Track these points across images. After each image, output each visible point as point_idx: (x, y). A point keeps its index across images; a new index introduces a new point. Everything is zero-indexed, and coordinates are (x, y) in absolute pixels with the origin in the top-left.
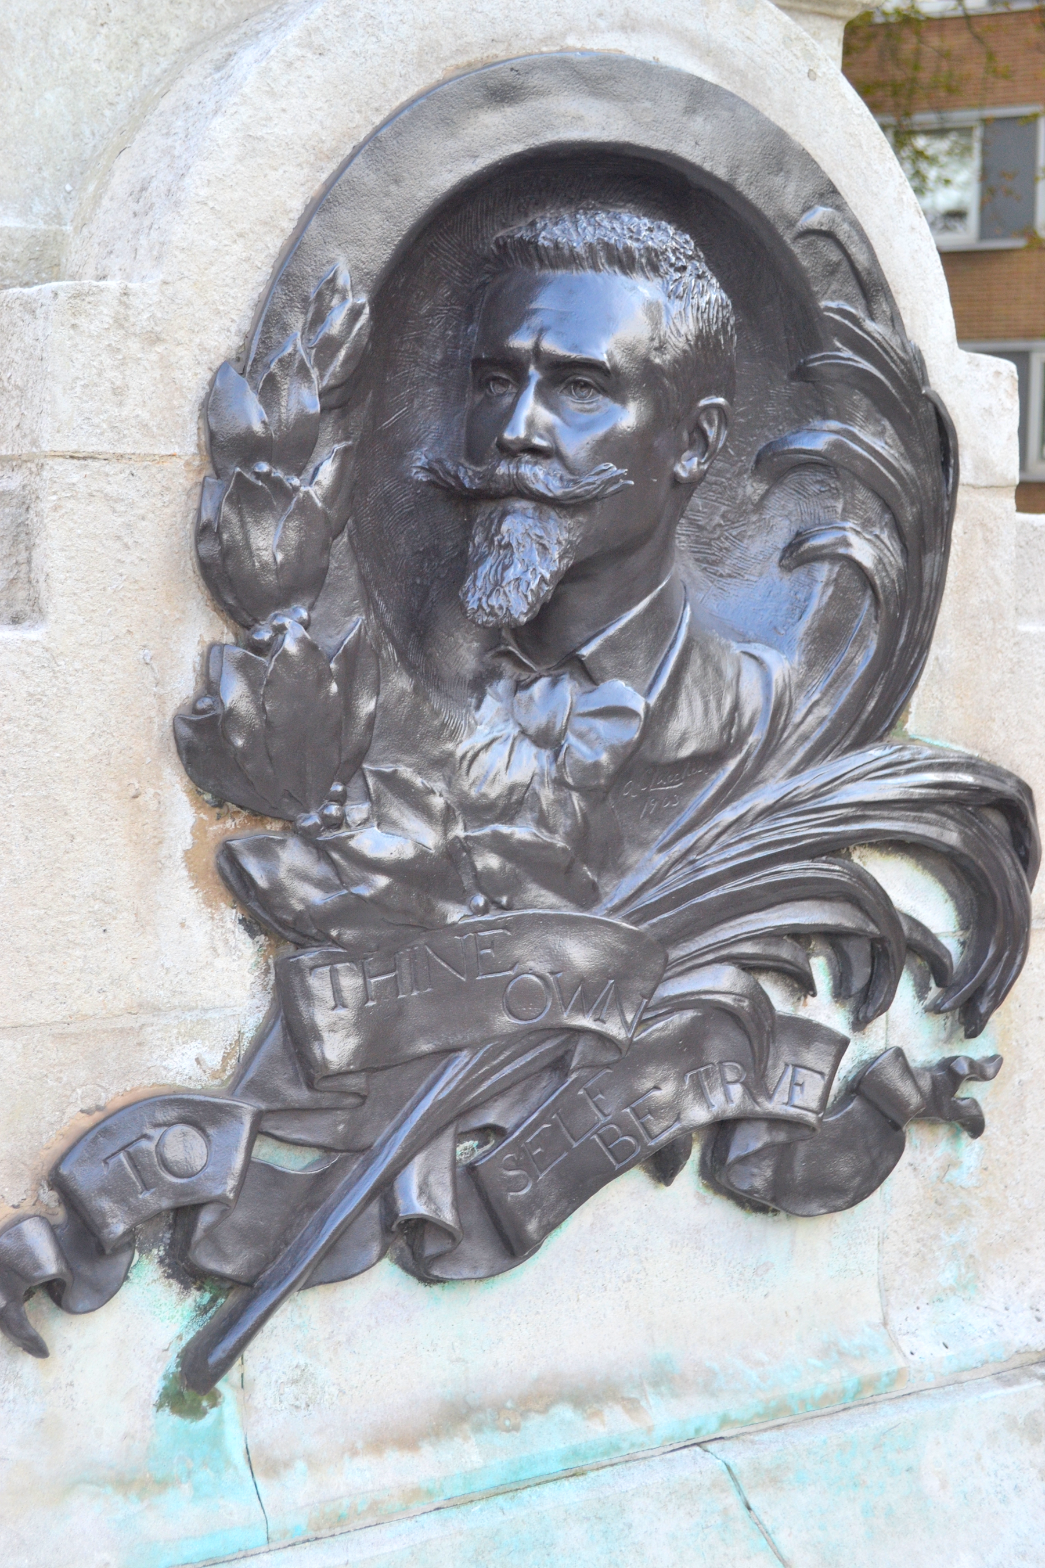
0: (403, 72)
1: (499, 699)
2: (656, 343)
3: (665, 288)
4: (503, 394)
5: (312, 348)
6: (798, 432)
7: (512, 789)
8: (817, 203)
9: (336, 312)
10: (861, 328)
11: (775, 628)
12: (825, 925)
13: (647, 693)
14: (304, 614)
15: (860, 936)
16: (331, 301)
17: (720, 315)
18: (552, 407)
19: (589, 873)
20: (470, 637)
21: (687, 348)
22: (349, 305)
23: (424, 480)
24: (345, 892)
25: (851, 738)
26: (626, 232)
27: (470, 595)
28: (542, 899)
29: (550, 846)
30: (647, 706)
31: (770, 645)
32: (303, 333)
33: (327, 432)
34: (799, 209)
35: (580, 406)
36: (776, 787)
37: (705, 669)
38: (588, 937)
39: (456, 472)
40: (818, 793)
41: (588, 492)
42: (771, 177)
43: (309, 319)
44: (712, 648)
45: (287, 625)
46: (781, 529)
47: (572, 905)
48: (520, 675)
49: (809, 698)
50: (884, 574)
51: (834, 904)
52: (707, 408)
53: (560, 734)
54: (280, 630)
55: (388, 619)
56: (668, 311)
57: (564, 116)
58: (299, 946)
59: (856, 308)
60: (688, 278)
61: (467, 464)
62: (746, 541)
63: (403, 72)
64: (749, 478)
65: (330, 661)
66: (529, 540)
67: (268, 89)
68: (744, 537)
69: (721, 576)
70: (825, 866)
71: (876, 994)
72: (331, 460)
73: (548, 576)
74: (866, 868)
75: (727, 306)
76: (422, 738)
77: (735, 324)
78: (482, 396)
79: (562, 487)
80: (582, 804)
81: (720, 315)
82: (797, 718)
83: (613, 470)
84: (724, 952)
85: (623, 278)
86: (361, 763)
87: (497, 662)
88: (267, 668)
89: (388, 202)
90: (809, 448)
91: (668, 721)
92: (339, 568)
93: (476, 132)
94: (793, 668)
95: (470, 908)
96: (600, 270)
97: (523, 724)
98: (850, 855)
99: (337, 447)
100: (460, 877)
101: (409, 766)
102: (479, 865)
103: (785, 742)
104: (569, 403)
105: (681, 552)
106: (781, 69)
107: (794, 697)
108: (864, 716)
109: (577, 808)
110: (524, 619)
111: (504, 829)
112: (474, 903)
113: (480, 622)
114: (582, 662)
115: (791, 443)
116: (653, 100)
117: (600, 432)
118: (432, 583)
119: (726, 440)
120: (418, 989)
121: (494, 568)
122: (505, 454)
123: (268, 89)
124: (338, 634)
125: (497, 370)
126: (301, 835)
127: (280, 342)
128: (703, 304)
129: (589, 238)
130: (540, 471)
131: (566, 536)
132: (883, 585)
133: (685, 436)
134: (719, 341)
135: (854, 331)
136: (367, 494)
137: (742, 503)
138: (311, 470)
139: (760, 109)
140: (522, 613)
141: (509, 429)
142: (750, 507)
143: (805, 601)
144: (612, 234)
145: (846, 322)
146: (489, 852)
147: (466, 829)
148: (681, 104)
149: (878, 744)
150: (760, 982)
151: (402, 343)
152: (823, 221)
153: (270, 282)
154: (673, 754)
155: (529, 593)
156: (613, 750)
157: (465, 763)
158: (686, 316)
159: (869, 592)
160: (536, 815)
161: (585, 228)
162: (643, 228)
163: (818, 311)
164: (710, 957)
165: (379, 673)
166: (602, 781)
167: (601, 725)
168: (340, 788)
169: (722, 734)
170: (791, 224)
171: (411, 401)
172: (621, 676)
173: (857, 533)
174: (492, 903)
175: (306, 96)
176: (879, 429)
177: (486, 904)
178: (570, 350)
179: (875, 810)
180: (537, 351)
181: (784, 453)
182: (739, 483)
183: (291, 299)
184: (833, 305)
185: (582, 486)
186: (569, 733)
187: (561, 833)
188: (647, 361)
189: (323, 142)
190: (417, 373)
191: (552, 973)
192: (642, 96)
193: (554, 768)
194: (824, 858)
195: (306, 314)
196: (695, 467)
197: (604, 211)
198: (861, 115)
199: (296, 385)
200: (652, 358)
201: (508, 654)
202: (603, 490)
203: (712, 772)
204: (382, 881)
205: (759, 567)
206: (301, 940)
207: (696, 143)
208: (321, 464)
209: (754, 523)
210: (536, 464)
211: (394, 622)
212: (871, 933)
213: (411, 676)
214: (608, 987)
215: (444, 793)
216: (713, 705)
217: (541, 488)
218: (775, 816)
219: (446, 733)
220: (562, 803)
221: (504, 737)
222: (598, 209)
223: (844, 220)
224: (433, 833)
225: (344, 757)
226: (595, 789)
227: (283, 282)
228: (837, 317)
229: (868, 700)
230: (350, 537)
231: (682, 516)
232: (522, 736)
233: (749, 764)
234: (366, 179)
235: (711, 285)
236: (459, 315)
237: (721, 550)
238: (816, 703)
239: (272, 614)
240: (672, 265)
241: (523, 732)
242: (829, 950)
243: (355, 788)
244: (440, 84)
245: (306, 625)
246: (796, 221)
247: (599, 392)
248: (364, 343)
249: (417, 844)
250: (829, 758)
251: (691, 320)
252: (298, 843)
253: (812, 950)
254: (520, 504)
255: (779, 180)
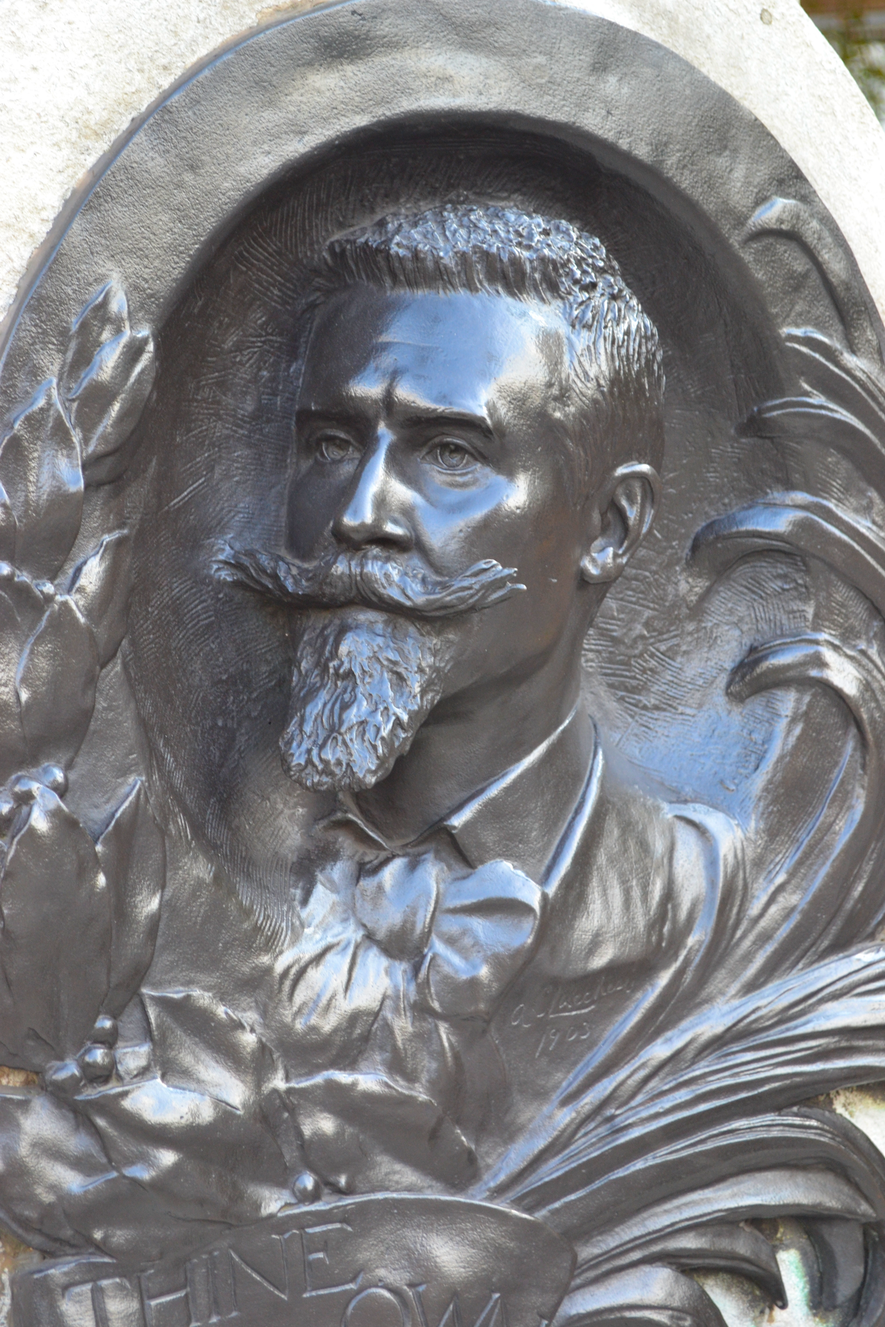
0: (201, 17)
1: (334, 888)
2: (555, 391)
3: (567, 314)
4: (341, 461)
5: (73, 400)
6: (750, 507)
7: (354, 1017)
8: (776, 194)
9: (107, 349)
10: (838, 364)
11: (722, 782)
12: (799, 1205)
13: (544, 880)
14: (59, 776)
15: (847, 1220)
16: (100, 334)
17: (644, 349)
18: (411, 480)
19: (463, 1138)
20: (292, 801)
21: (599, 396)
22: (125, 339)
23: (229, 579)
24: (114, 1174)
25: (830, 937)
26: (512, 237)
27: (295, 744)
28: (396, 1177)
29: (408, 1101)
30: (544, 896)
31: (715, 807)
32: (60, 379)
33: (93, 519)
34: (750, 202)
35: (449, 479)
36: (726, 1008)
37: (625, 842)
38: (462, 1231)
39: (274, 569)
40: (785, 1016)
41: (462, 600)
42: (711, 157)
43: (69, 360)
44: (633, 811)
45: (36, 793)
46: (728, 642)
47: (438, 1185)
48: (364, 854)
49: (771, 881)
50: (873, 705)
51: (810, 1175)
52: (626, 478)
53: (421, 938)
54: (25, 799)
55: (178, 779)
56: (571, 345)
57: (425, 76)
58: (46, 1254)
59: (830, 336)
60: (599, 300)
61: (289, 558)
62: (679, 659)
63: (201, 17)
64: (683, 570)
65: (96, 842)
66: (378, 667)
67: (13, 39)
68: (676, 653)
69: (645, 708)
70: (797, 1121)
71: (872, 1303)
72: (98, 557)
73: (405, 718)
74: (853, 1121)
75: (653, 335)
76: (225, 948)
77: (663, 360)
78: (311, 462)
79: (426, 593)
80: (453, 1039)
81: (644, 349)
82: (754, 909)
83: (497, 569)
84: (656, 1248)
85: (510, 300)
86: (139, 987)
87: (331, 835)
88: (7, 854)
89: (181, 196)
90: (767, 529)
91: (574, 918)
92: (109, 709)
93: (304, 99)
94: (747, 839)
95: (294, 1193)
96: (477, 290)
97: (369, 925)
98: (831, 1103)
99: (107, 538)
100: (280, 1148)
101: (207, 989)
102: (307, 1130)
103: (738, 944)
104: (435, 474)
105: (589, 674)
106: (724, 9)
107: (749, 880)
108: (849, 905)
109: (446, 1044)
110: (372, 780)
111: (343, 1077)
112: (299, 1185)
113: (309, 783)
114: (452, 836)
115: (741, 523)
116: (550, 55)
117: (478, 514)
118: (239, 724)
119: (653, 521)
120: (218, 1314)
121: (329, 706)
122: (344, 546)
123: (13, 39)
124: (108, 801)
125: (331, 427)
126: (52, 1094)
127: (27, 393)
128: (620, 336)
129: (461, 246)
130: (394, 571)
131: (430, 660)
132: (872, 718)
133: (596, 517)
134: (642, 386)
135: (828, 369)
136: (148, 602)
137: (674, 606)
138: (71, 572)
139: (696, 64)
140: (369, 771)
141: (350, 511)
142: (685, 611)
143: (763, 744)
144: (493, 240)
145: (817, 356)
146: (321, 1111)
147: (287, 1079)
148: (586, 58)
149: (868, 944)
150: (707, 1289)
151: (198, 389)
152: (784, 217)
153: (14, 308)
154: (581, 965)
155: (379, 743)
156: (496, 961)
157: (288, 983)
158: (597, 352)
159: (853, 731)
160: (387, 1055)
161: (455, 231)
162: (536, 230)
163: (778, 341)
164: (636, 1255)
165: (165, 857)
166: (482, 1006)
167: (479, 925)
168: (108, 1024)
169: (649, 935)
170: (741, 221)
171: (211, 469)
172: (507, 855)
173: (836, 648)
174: (327, 1185)
175: (67, 49)
176: (864, 502)
177: (317, 1186)
178: (436, 400)
179: (865, 1039)
180: (389, 402)
181: (731, 536)
182: (668, 579)
183: (45, 332)
184: (798, 332)
185: (454, 592)
186: (434, 938)
187: (424, 1081)
188: (542, 415)
189: (89, 113)
190: (220, 429)
191: (411, 1285)
192: (533, 48)
193: (413, 988)
194: (795, 1109)
195: (64, 353)
196: (610, 560)
197: (480, 205)
198: (834, 72)
199: (49, 452)
200: (550, 411)
201: (348, 825)
202: (484, 597)
203: (635, 990)
204: (168, 1158)
205: (698, 695)
206: (51, 1246)
207: (609, 112)
208: (85, 563)
209: (691, 634)
210: (388, 559)
211: (187, 782)
212: (864, 1215)
213: (210, 860)
214: (491, 1304)
215: (257, 1027)
216: (636, 893)
217: (395, 594)
218: (725, 1050)
219: (260, 940)
220: (424, 1038)
221: (342, 944)
222: (471, 202)
223: (812, 216)
224: (241, 1085)
225: (114, 980)
226: (472, 1018)
227: (31, 309)
228: (804, 349)
229: (854, 882)
230: (125, 666)
231: (591, 625)
232: (367, 942)
233: (688, 977)
234: (150, 164)
235: (630, 308)
236: (279, 348)
237: (644, 671)
238: (780, 889)
239: (13, 777)
240: (576, 282)
241: (370, 937)
242: (804, 1240)
243: (130, 1022)
244: (254, 32)
245: (62, 791)
246: (747, 218)
247: (476, 459)
248: (147, 393)
249: (218, 1103)
250: (800, 966)
251: (603, 357)
252: (47, 1104)
253: (781, 1240)
254: (365, 616)
255: (722, 162)
